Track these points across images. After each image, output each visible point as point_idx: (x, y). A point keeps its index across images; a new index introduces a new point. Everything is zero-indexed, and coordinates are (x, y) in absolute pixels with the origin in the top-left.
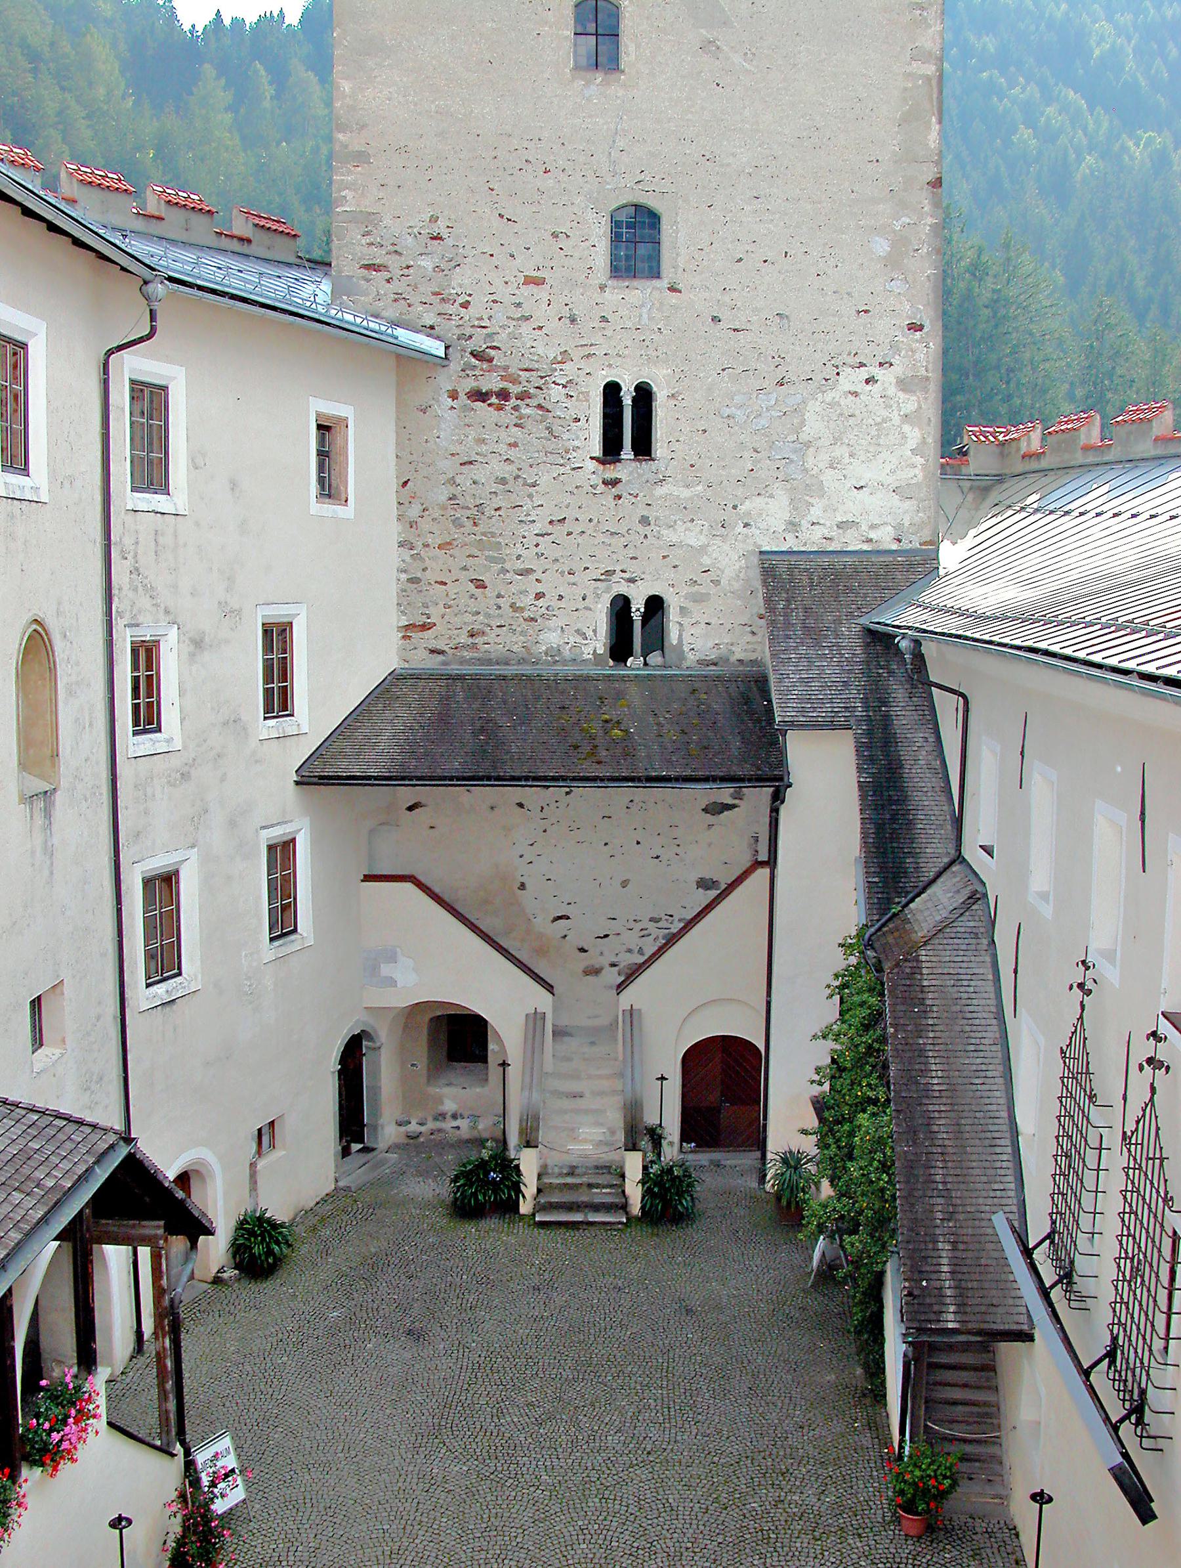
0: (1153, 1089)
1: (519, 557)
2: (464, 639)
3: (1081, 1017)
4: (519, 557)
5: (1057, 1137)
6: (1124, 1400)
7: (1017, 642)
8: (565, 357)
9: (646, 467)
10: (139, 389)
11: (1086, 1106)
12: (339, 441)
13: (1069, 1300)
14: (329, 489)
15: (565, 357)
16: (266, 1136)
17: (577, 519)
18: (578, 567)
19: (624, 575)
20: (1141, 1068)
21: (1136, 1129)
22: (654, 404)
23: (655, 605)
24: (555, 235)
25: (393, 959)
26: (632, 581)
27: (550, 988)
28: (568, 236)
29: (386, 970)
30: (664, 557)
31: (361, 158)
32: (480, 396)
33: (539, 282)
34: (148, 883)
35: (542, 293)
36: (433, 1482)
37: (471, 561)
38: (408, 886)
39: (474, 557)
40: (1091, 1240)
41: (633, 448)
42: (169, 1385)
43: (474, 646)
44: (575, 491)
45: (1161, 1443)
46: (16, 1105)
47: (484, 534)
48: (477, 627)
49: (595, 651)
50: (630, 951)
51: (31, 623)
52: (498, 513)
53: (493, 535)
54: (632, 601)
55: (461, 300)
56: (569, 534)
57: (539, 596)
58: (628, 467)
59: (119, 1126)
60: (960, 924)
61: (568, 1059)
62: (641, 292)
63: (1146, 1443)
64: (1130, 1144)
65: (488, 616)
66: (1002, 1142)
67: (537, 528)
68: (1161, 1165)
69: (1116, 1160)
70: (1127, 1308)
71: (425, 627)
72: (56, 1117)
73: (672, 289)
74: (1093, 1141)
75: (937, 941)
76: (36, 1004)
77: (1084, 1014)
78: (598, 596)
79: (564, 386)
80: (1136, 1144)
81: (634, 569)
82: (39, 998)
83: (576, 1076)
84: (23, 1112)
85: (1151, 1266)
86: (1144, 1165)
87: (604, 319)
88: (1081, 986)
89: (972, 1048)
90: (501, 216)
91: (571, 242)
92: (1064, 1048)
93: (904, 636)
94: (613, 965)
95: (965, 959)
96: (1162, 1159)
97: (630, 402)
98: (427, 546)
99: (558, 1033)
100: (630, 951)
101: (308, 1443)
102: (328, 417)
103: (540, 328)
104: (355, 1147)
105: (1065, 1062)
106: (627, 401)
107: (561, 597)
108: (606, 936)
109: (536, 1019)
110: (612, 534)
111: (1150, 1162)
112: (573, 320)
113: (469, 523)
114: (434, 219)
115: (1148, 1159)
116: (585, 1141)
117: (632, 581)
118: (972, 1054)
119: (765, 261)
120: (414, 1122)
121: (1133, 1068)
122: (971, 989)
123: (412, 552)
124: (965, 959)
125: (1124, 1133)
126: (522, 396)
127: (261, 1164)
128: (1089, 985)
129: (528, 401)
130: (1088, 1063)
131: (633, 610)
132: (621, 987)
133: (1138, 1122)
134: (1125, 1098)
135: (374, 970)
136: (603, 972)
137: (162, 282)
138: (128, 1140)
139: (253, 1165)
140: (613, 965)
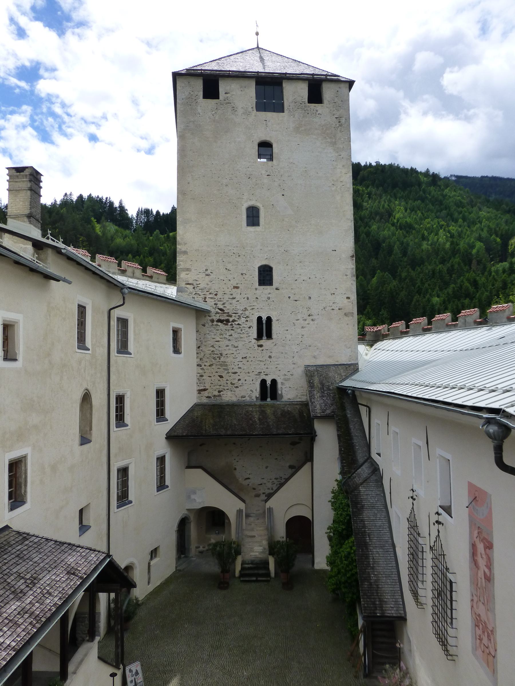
0: (439, 532)
1: (233, 369)
2: (216, 393)
3: (413, 508)
4: (233, 369)
5: (408, 548)
6: (439, 642)
7: (384, 390)
8: (246, 309)
9: (270, 341)
10: (119, 319)
11: (417, 537)
12: (179, 335)
13: (417, 605)
14: (176, 350)
15: (246, 309)
16: (154, 553)
17: (250, 357)
18: (250, 371)
19: (264, 373)
20: (434, 524)
21: (434, 545)
22: (272, 322)
23: (274, 382)
24: (242, 274)
25: (195, 493)
26: (267, 375)
27: (244, 501)
28: (246, 274)
29: (193, 497)
30: (276, 368)
31: (185, 253)
32: (220, 321)
33: (237, 288)
34: (119, 470)
35: (238, 291)
36: (207, 676)
37: (218, 370)
38: (200, 471)
39: (219, 369)
40: (423, 584)
41: (266, 336)
42: (119, 643)
43: (220, 396)
44: (249, 349)
45: (455, 658)
46: (74, 545)
47: (222, 362)
48: (220, 390)
49: (256, 396)
50: (269, 489)
51: (85, 390)
52: (226, 355)
53: (225, 362)
54: (267, 381)
55: (215, 293)
56: (248, 361)
57: (239, 380)
58: (264, 342)
59: (106, 551)
60: (372, 478)
61: (250, 525)
62: (267, 289)
63: (449, 657)
64: (433, 550)
65: (224, 386)
66: (390, 550)
67: (238, 360)
68: (444, 557)
69: (428, 556)
70: (437, 608)
71: (205, 390)
72: (87, 549)
73: (277, 289)
74: (420, 549)
75: (364, 484)
76: (81, 511)
77: (414, 507)
78: (257, 380)
79: (246, 318)
80: (435, 550)
81: (267, 372)
82: (82, 509)
83: (252, 530)
84: (76, 548)
85: (444, 592)
86: (438, 557)
87: (257, 298)
88: (412, 497)
89: (378, 518)
90: (226, 269)
91: (247, 276)
92: (408, 518)
93: (349, 389)
94: (264, 493)
95: (374, 489)
96: (444, 555)
97: (265, 322)
98: (205, 365)
99: (247, 516)
100: (269, 489)
101: (165, 663)
102: (176, 328)
103: (238, 301)
104: (183, 556)
105: (409, 523)
106: (264, 322)
107: (246, 380)
108: (261, 484)
109: (240, 512)
110: (260, 361)
111: (440, 556)
112: (248, 299)
113: (218, 359)
114: (206, 270)
115: (439, 555)
116: (256, 552)
117: (267, 375)
118: (378, 520)
119: (304, 280)
120: (201, 547)
121: (432, 524)
122: (377, 499)
123: (201, 368)
124: (374, 489)
125: (430, 546)
126: (234, 321)
127: (152, 563)
128: (415, 497)
129: (235, 322)
130: (416, 523)
131: (267, 383)
132: (266, 501)
133: (435, 542)
134: (429, 534)
135: (189, 497)
136: (261, 496)
137: (127, 289)
138: (108, 555)
139: (149, 564)
140: (264, 493)
